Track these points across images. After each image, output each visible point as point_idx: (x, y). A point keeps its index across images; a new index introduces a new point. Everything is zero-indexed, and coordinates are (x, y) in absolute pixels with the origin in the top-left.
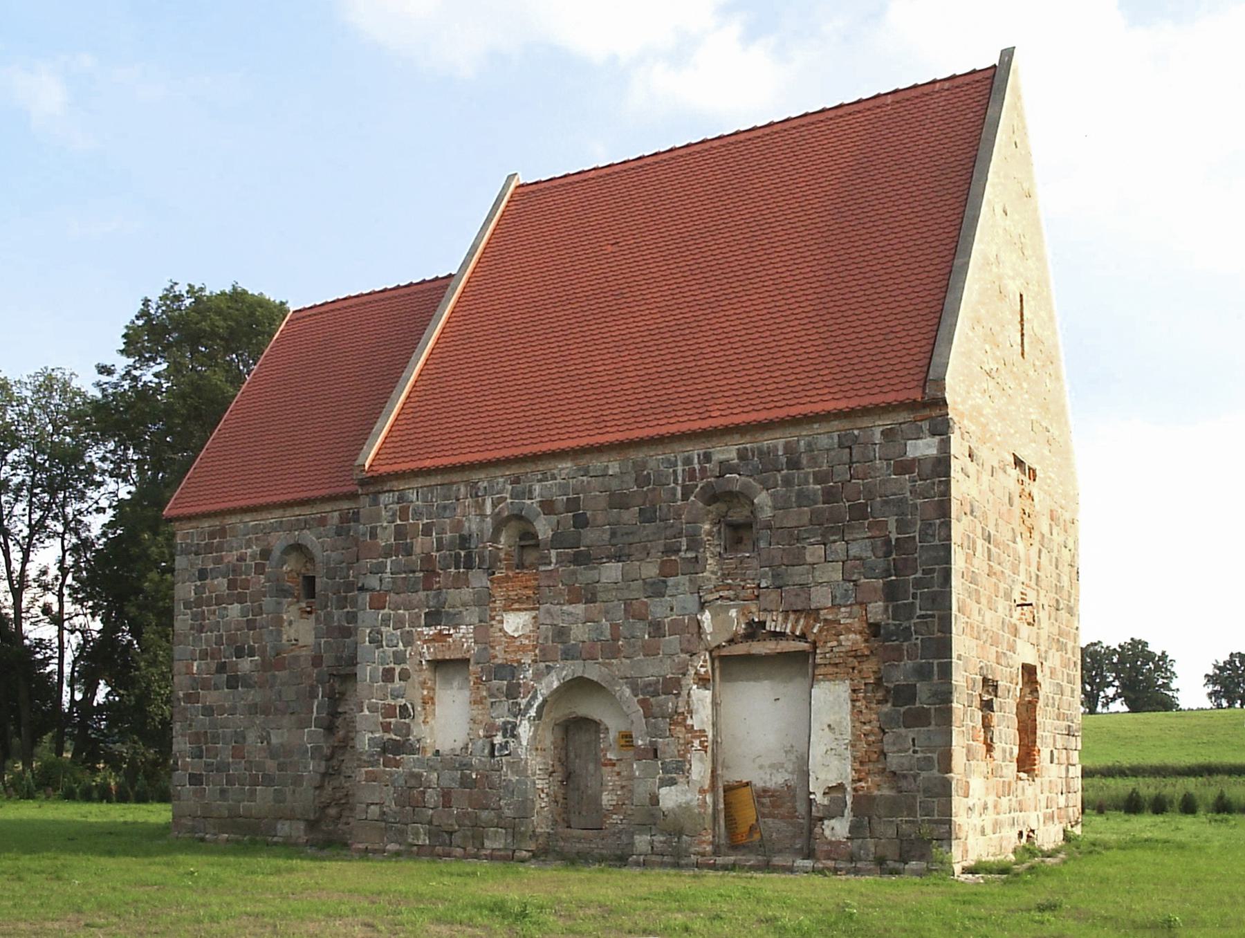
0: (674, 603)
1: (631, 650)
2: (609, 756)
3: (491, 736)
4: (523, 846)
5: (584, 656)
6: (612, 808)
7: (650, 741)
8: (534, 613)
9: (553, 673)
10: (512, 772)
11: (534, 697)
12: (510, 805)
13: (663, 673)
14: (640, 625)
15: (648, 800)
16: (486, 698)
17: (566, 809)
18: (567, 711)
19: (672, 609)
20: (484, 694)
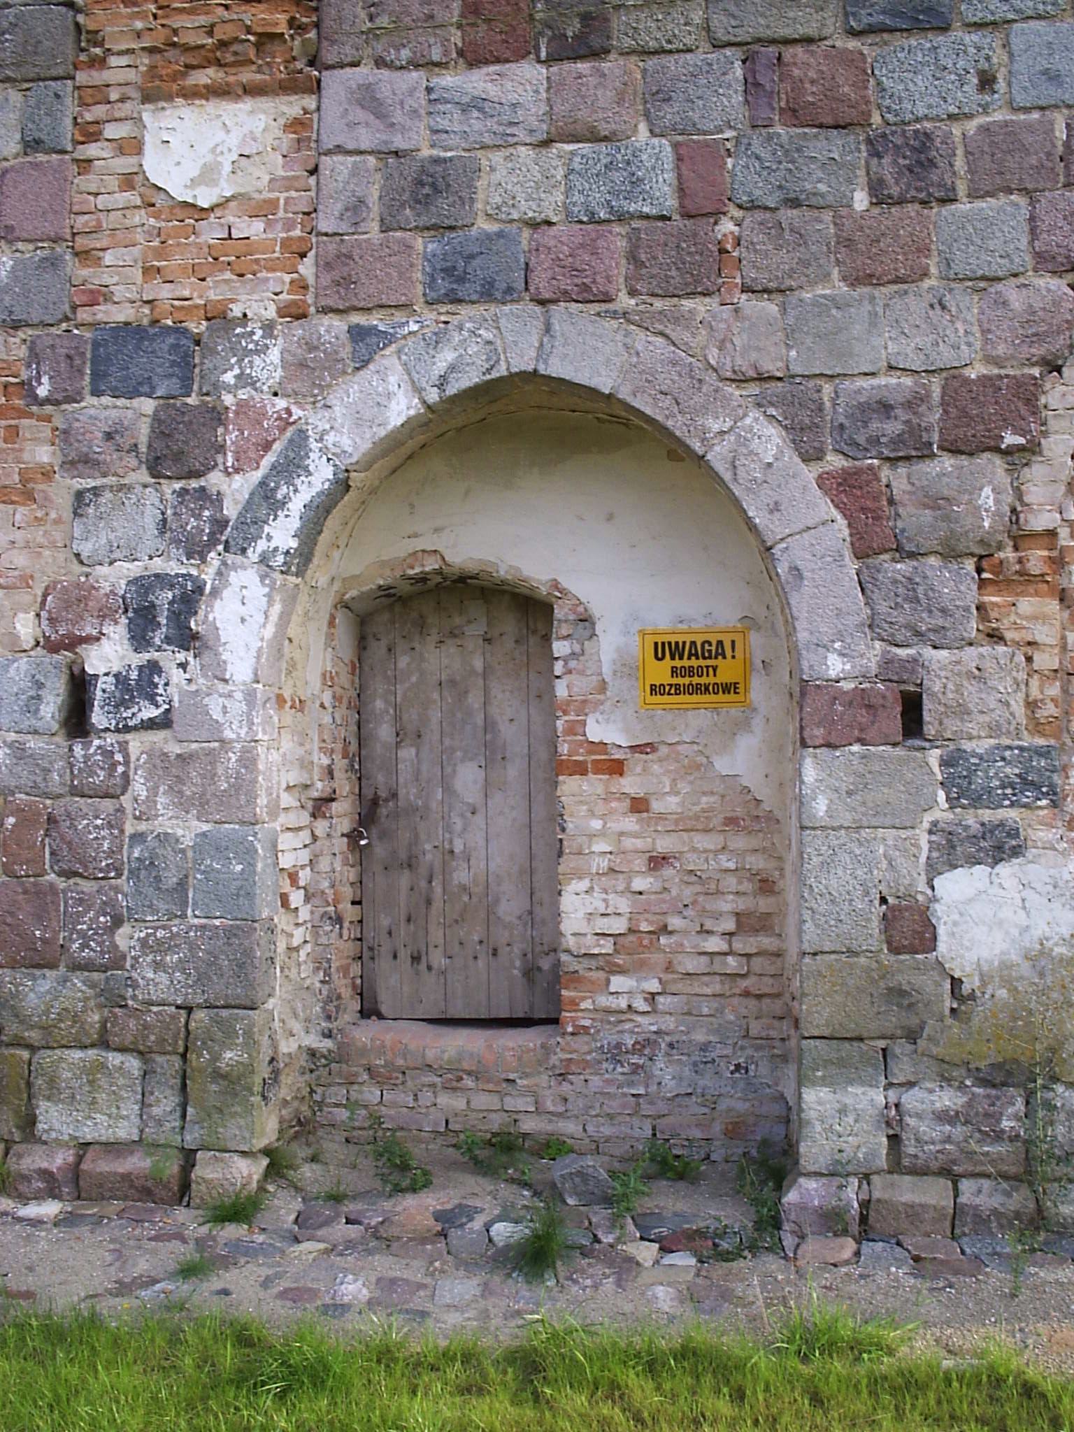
0: (999, 57)
1: (783, 260)
2: (596, 730)
3: (73, 642)
4: (231, 1131)
5: (541, 281)
6: (607, 947)
7: (887, 662)
8: (293, 106)
9: (388, 360)
10: (183, 805)
11: (292, 466)
12: (162, 947)
13: (946, 357)
14: (834, 146)
15: (875, 925)
16: (47, 474)
17: (365, 953)
18: (404, 548)
19: (986, 82)
20: (44, 455)
